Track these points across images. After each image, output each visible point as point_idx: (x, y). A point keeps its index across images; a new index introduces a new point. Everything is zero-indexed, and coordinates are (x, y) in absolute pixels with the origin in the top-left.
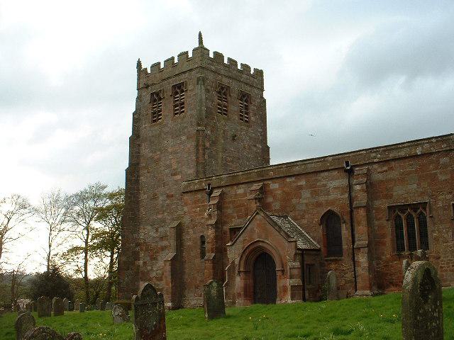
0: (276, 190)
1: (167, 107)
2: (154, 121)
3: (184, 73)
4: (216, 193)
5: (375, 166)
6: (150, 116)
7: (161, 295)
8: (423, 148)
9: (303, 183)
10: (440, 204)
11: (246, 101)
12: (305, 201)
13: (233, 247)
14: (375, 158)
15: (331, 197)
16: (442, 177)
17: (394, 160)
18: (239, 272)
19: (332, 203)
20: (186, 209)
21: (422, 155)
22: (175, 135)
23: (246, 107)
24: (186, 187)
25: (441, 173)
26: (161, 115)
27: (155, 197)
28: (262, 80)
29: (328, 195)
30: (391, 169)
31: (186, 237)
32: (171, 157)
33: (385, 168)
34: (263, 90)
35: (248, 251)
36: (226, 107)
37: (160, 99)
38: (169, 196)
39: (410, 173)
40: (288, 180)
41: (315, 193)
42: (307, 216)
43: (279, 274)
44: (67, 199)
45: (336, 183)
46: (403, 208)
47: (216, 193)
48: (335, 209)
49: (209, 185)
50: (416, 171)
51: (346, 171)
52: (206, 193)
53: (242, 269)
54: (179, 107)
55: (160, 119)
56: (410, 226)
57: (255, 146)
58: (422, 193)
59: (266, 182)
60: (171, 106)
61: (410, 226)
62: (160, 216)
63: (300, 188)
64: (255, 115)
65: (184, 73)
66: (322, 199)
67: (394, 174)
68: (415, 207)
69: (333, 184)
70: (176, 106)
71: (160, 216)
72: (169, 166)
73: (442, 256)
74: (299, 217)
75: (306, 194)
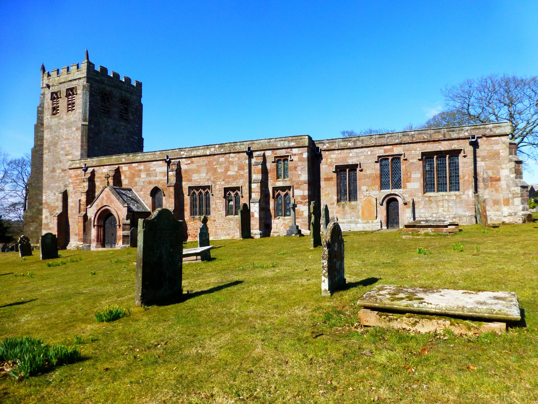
0: (126, 171)
1: (63, 103)
2: (54, 114)
3: (75, 80)
4: (90, 170)
5: (184, 160)
6: (50, 111)
7: (484, 201)
8: (210, 151)
9: (142, 167)
10: (217, 187)
11: (126, 104)
12: (143, 180)
13: (91, 209)
14: (183, 154)
15: (157, 178)
16: (219, 171)
17: (194, 157)
18: (94, 226)
19: (159, 182)
20: (70, 180)
21: (210, 155)
22: (68, 126)
23: (126, 109)
24: (71, 165)
25: (219, 168)
26: (58, 110)
27: (54, 170)
28: (141, 90)
29: (156, 176)
30: (192, 162)
31: (70, 200)
32: (65, 142)
33: (189, 162)
34: (141, 96)
35: (99, 212)
36: (108, 108)
37: (58, 98)
38: (64, 170)
39: (202, 166)
40: (134, 165)
41: (148, 175)
42: (143, 190)
43: (118, 227)
44: (483, 88)
45: (159, 170)
46: (197, 188)
47: (90, 170)
48: (160, 186)
49: (85, 165)
50: (206, 165)
51: (166, 162)
52: (83, 170)
53: (96, 224)
54: (71, 106)
55: (58, 113)
56: (201, 200)
57: (132, 137)
58: (208, 180)
59: (120, 165)
60: (65, 104)
61: (201, 200)
62: (57, 184)
63: (140, 171)
64: (133, 115)
65: (75, 80)
66: (153, 179)
67: (193, 166)
68: (204, 188)
69: (159, 170)
70: (69, 104)
71: (57, 184)
72: (63, 149)
73: (217, 220)
74: (139, 190)
75: (143, 175)
